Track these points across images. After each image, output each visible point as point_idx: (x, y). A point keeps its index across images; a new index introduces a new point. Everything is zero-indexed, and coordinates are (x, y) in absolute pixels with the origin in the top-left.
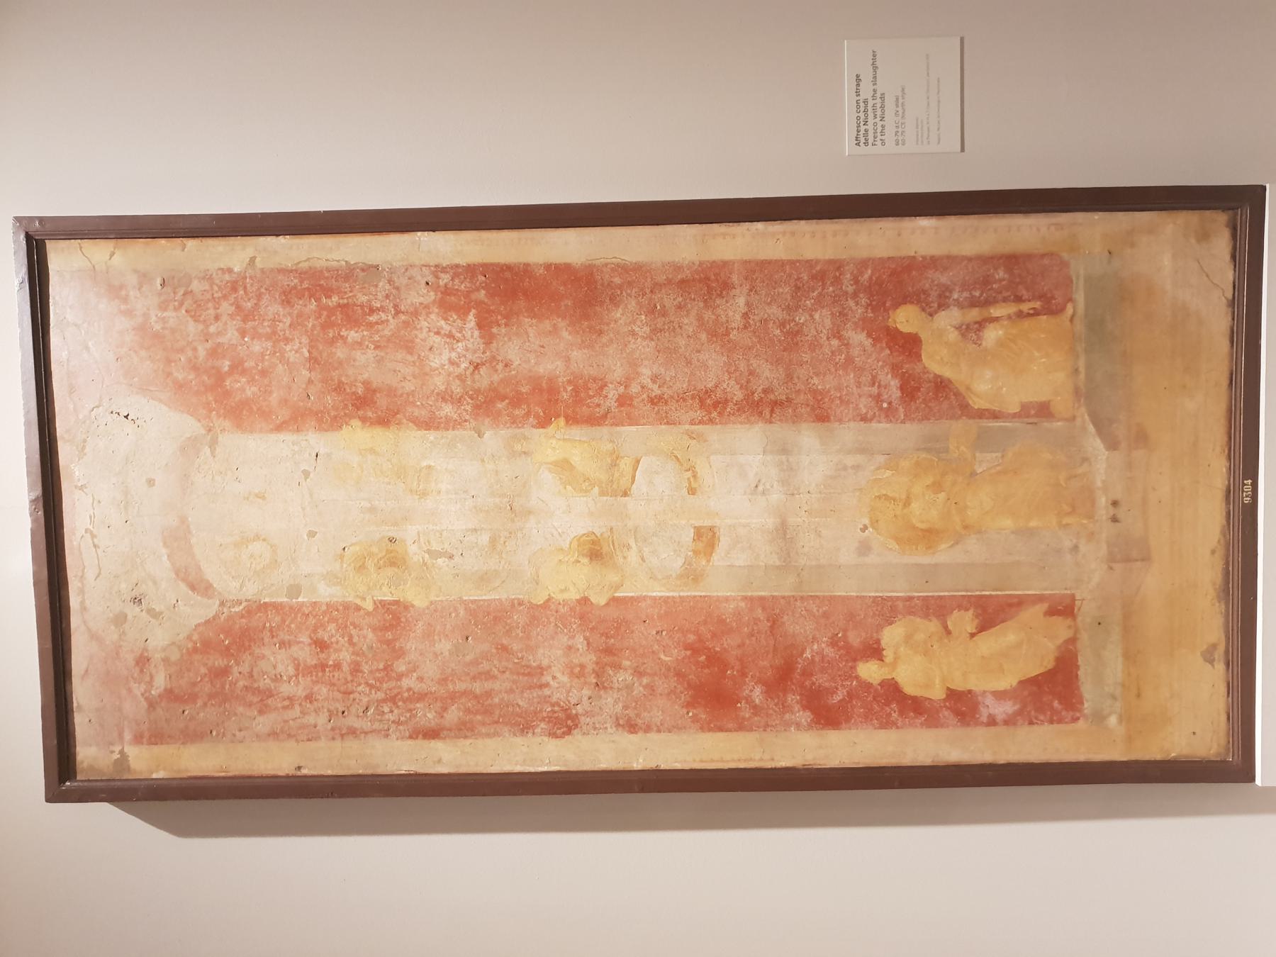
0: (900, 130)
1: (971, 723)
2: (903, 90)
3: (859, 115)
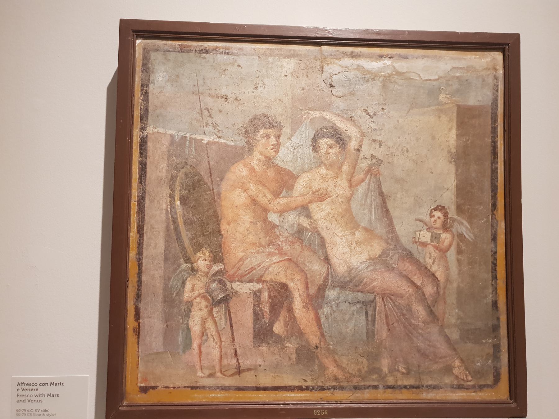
0: (26, 412)
1: (441, 253)
2: (53, 415)
3: (38, 385)
